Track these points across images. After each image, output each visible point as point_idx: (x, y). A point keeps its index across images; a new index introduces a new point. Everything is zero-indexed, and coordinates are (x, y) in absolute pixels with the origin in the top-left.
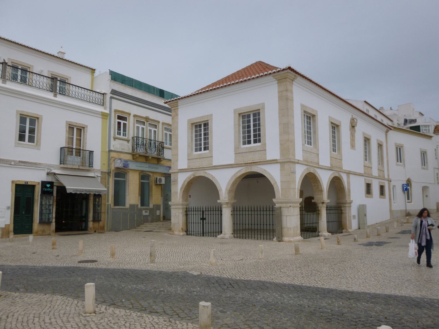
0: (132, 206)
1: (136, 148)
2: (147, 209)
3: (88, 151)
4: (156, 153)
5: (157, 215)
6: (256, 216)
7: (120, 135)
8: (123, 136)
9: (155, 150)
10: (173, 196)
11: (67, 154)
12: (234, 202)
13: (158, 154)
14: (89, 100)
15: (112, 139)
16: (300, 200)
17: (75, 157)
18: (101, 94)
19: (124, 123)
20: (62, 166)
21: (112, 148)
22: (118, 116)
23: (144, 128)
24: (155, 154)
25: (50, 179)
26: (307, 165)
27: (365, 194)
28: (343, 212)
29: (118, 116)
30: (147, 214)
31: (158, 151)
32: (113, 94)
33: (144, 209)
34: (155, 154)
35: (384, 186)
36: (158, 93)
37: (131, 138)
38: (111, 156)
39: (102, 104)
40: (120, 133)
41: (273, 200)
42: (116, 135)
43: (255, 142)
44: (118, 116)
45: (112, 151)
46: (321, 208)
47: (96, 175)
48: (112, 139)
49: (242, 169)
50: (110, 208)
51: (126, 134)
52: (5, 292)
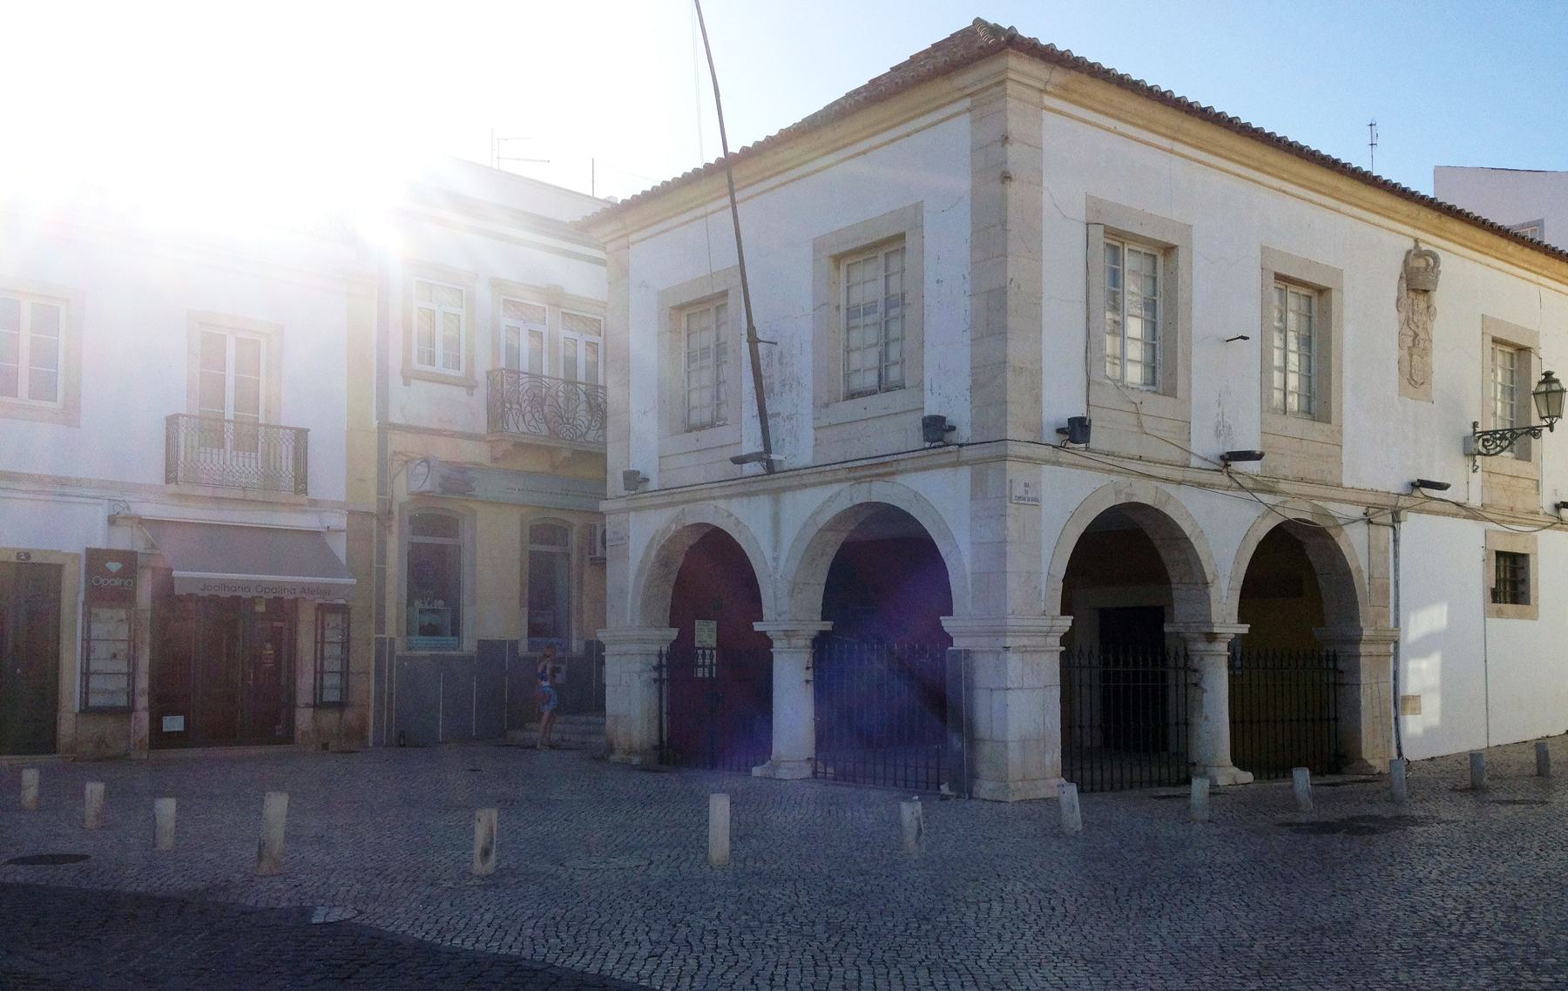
0: (489, 649)
3: (291, 429)
9: (590, 424)
11: (196, 444)
17: (234, 453)
20: (172, 488)
25: (123, 540)
28: (1345, 681)
45: (395, 427)
46: (1202, 659)
47: (326, 525)
49: (839, 494)
50: (392, 652)
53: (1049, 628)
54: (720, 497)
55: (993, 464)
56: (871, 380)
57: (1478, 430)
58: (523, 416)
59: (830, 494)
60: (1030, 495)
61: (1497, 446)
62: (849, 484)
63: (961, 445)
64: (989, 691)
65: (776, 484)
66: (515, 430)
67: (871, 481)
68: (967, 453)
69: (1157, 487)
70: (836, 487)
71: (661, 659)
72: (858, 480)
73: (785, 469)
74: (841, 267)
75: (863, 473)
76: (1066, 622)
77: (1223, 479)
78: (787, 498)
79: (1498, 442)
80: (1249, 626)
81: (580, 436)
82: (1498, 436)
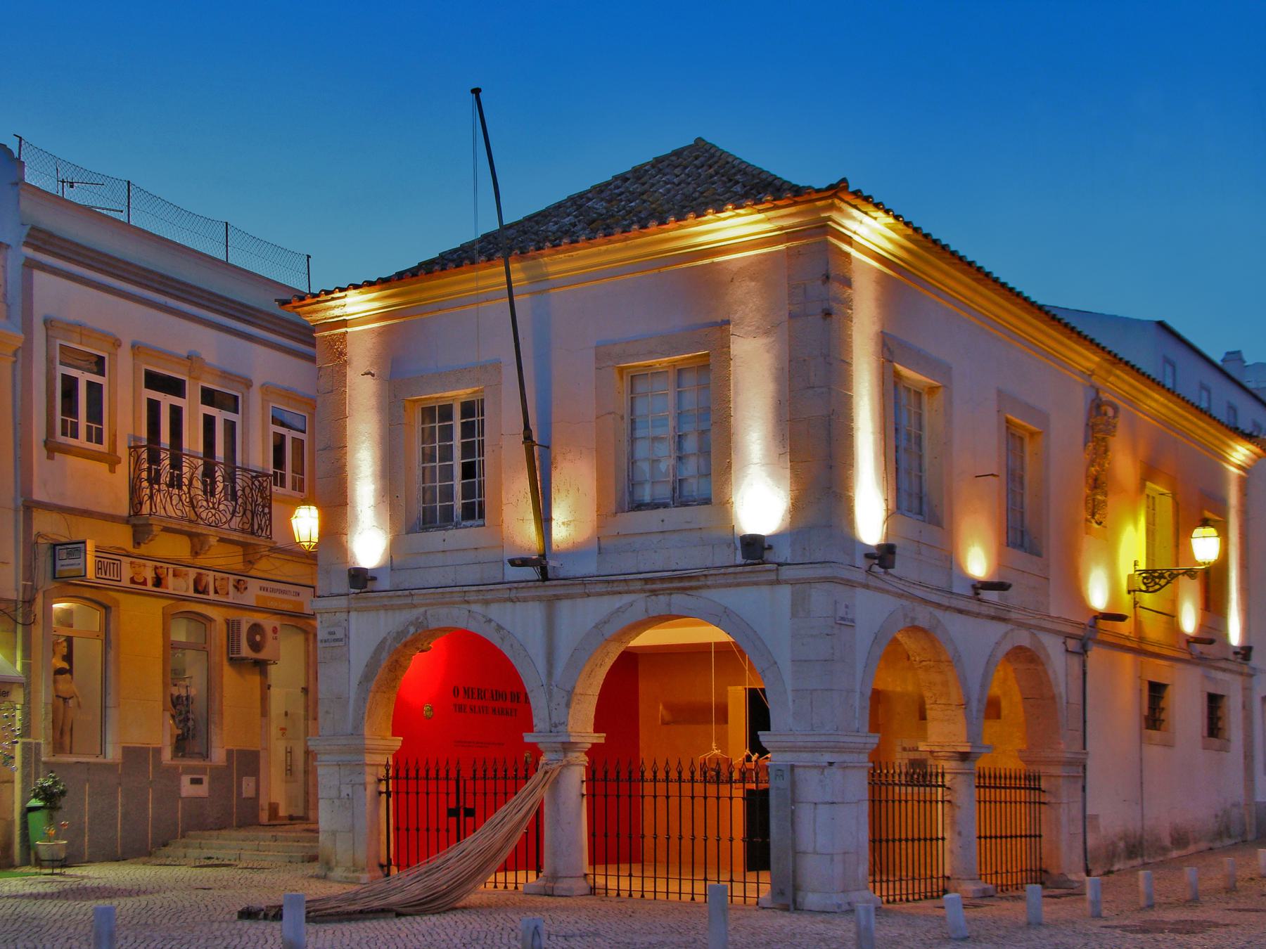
1: (151, 497)
4: (236, 522)
5: (244, 795)
6: (686, 802)
8: (89, 439)
10: (327, 712)
13: (246, 526)
15: (38, 452)
16: (869, 740)
19: (90, 384)
21: (39, 495)
23: (234, 423)
24: (233, 524)
26: (901, 596)
27: (1203, 737)
29: (146, 370)
30: (202, 790)
31: (244, 513)
32: (37, 248)
33: (188, 770)
34: (233, 524)
35: (1222, 696)
36: (1246, 645)
37: (123, 451)
38: (35, 532)
40: (75, 427)
41: (761, 739)
42: (54, 438)
43: (446, 412)
48: (38, 452)
51: (100, 432)
52: (857, 902)
54: (475, 602)
55: (818, 585)
56: (664, 492)
57: (1138, 568)
58: (171, 498)
59: (617, 605)
61: (1156, 584)
63: (779, 565)
64: (812, 806)
67: (671, 594)
68: (786, 573)
69: (931, 613)
70: (627, 599)
71: (388, 771)
72: (654, 592)
78: (564, 607)
79: (1157, 580)
80: (605, 735)
82: (1156, 574)
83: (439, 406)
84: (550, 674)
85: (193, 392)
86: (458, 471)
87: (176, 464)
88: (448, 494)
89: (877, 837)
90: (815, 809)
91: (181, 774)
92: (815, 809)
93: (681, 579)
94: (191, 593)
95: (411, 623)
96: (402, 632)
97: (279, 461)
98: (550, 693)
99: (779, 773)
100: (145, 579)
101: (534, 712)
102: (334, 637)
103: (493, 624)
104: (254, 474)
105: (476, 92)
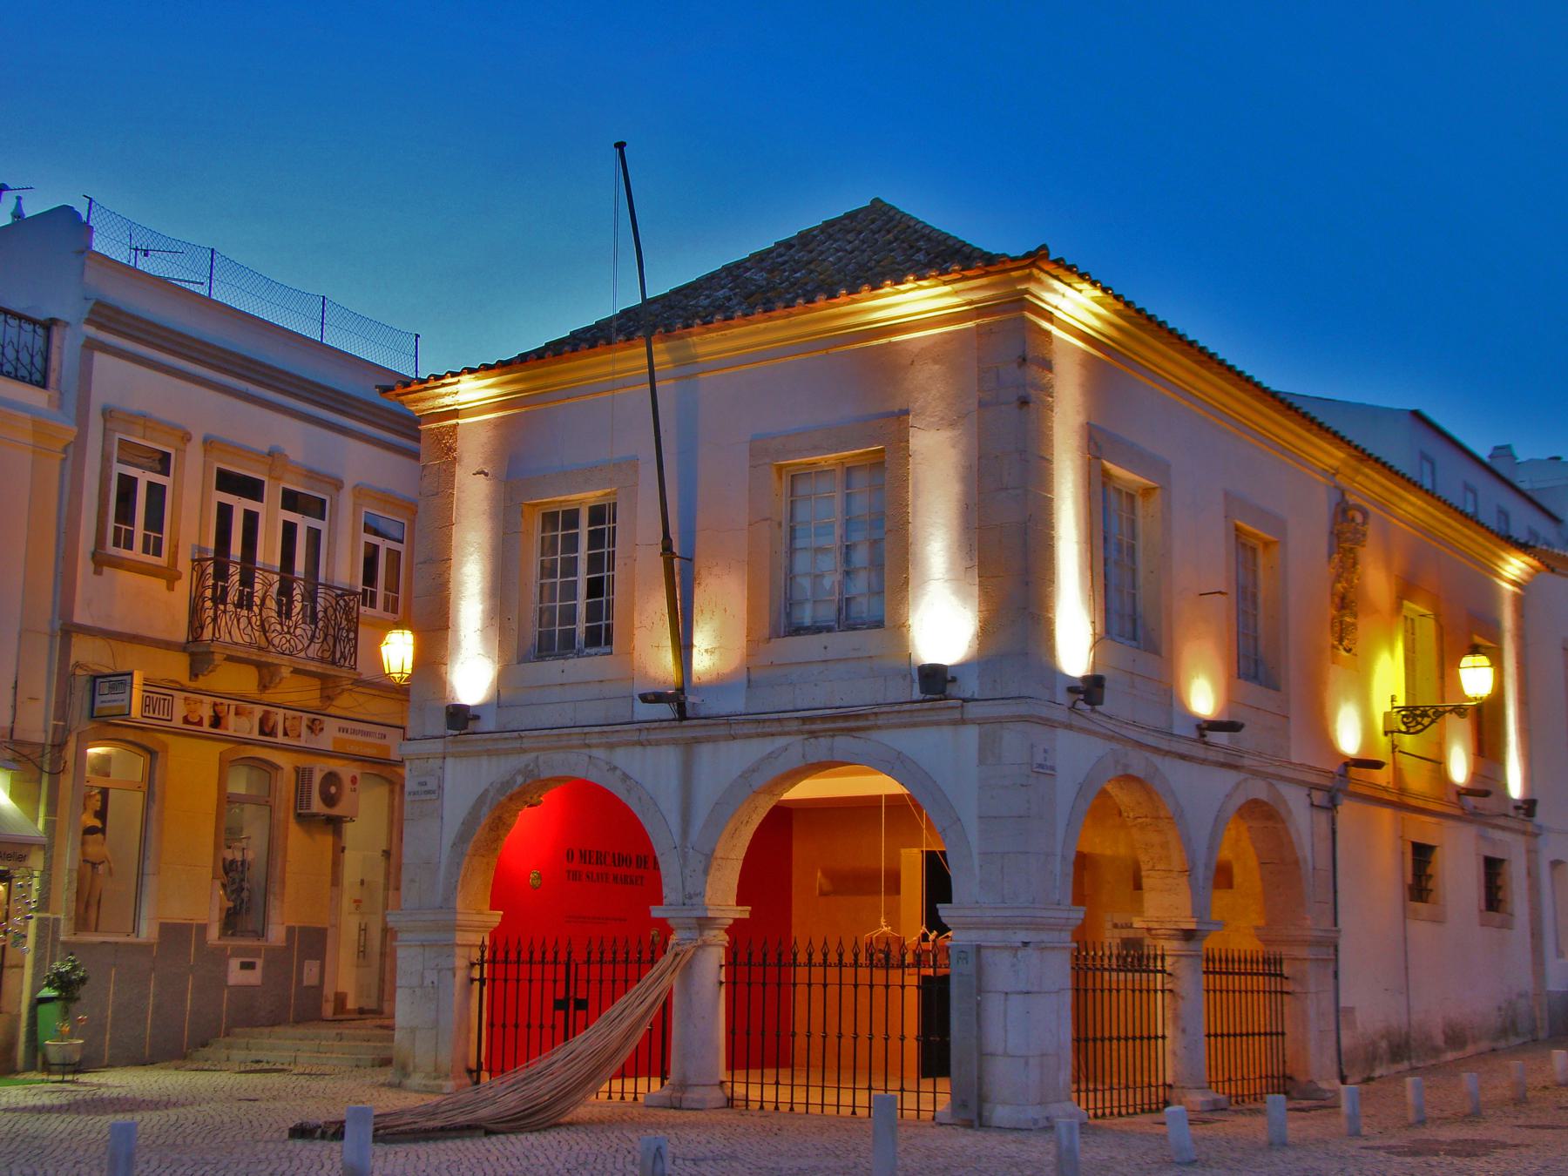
0: (173, 934)
1: (215, 620)
2: (256, 952)
4: (314, 650)
6: (848, 991)
7: (131, 548)
8: (146, 550)
9: (313, 636)
10: (412, 881)
12: (738, 916)
14: (26, 374)
15: (84, 565)
18: (34, 322)
19: (151, 485)
21: (80, 617)
22: (221, 473)
24: (311, 652)
26: (1110, 738)
30: (254, 977)
31: (325, 639)
32: (100, 327)
33: (237, 952)
37: (184, 565)
38: (72, 662)
39: (37, 376)
40: (130, 535)
44: (221, 473)
48: (84, 565)
53: (1064, 921)
57: (1396, 704)
58: (238, 620)
60: (1048, 763)
62: (802, 737)
63: (965, 700)
64: (1003, 997)
65: (689, 733)
66: (228, 639)
68: (973, 710)
70: (781, 742)
71: (483, 952)
72: (813, 734)
73: (702, 715)
74: (784, 477)
75: (827, 726)
76: (496, 917)
77: (1198, 750)
78: (705, 752)
79: (1419, 719)
80: (750, 908)
81: (301, 650)
82: (1418, 712)
83: (563, 511)
84: (685, 832)
85: (273, 494)
86: (582, 589)
87: (247, 580)
88: (569, 615)
89: (1082, 1036)
90: (1006, 1000)
91: (230, 957)
92: (1006, 1000)
93: (846, 717)
94: (255, 735)
95: (519, 772)
96: (508, 782)
97: (370, 577)
98: (684, 856)
99: (963, 955)
100: (201, 719)
101: (664, 880)
102: (425, 788)
103: (618, 773)
104: (339, 592)
105: (620, 146)
